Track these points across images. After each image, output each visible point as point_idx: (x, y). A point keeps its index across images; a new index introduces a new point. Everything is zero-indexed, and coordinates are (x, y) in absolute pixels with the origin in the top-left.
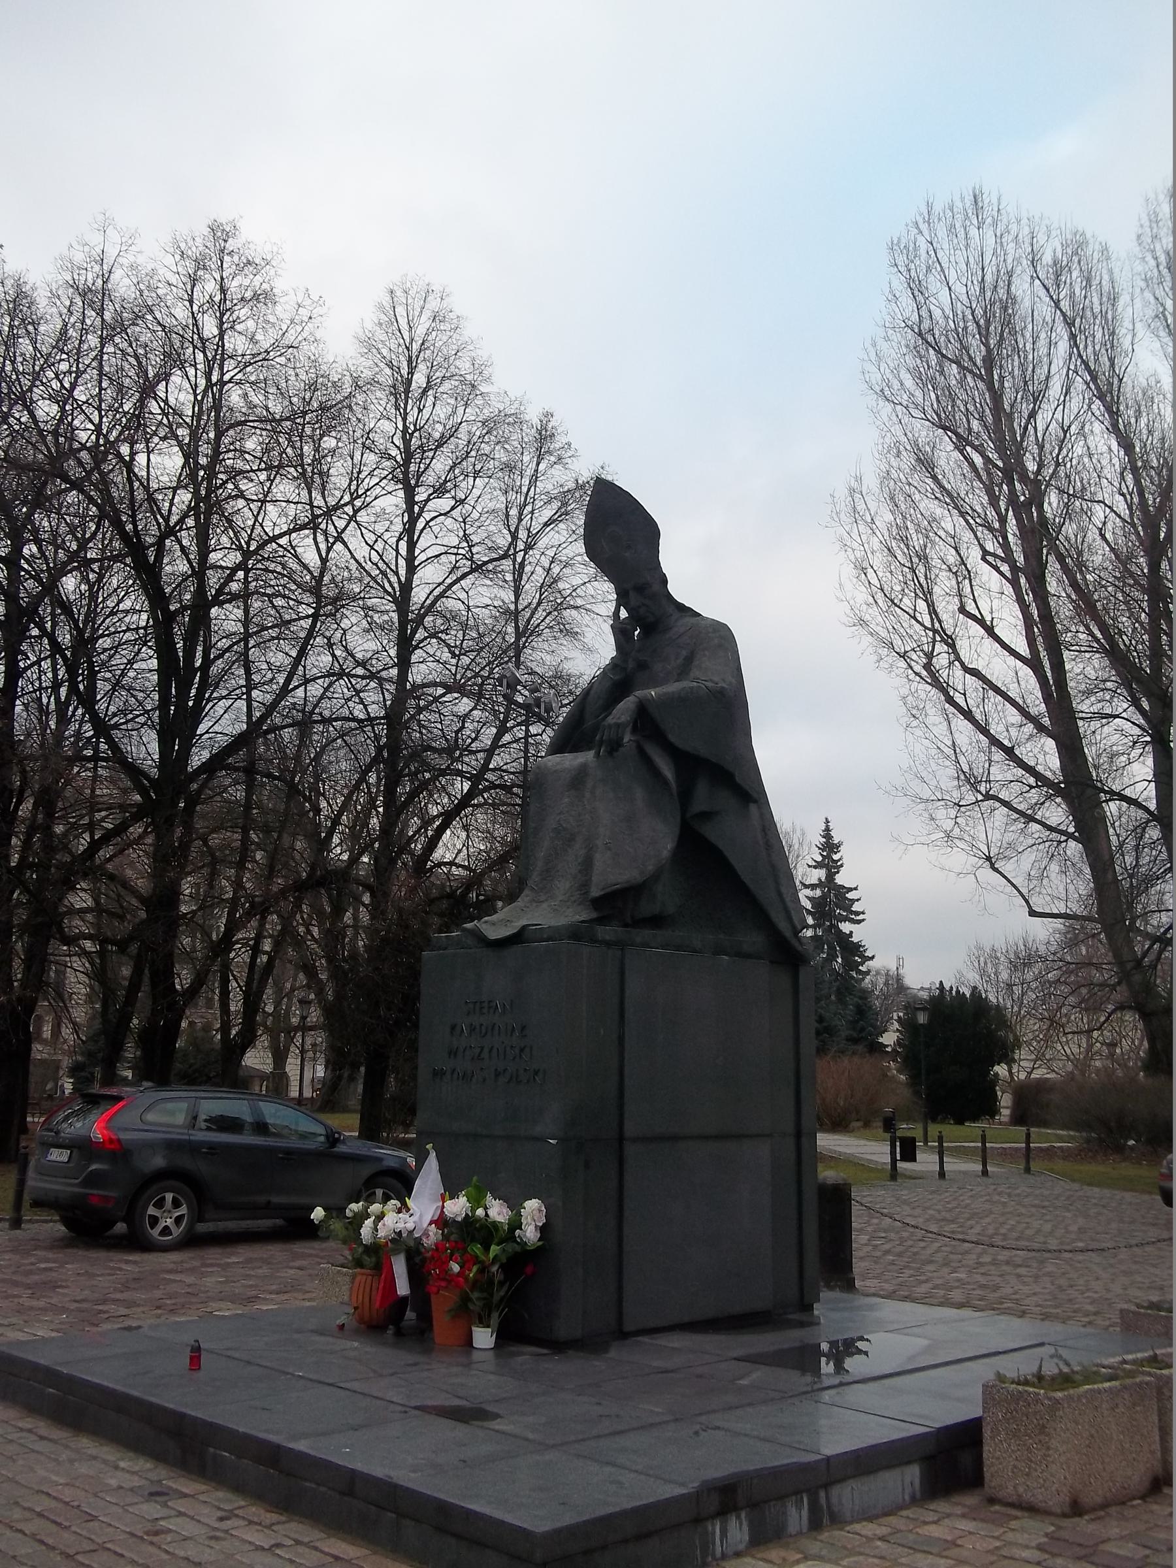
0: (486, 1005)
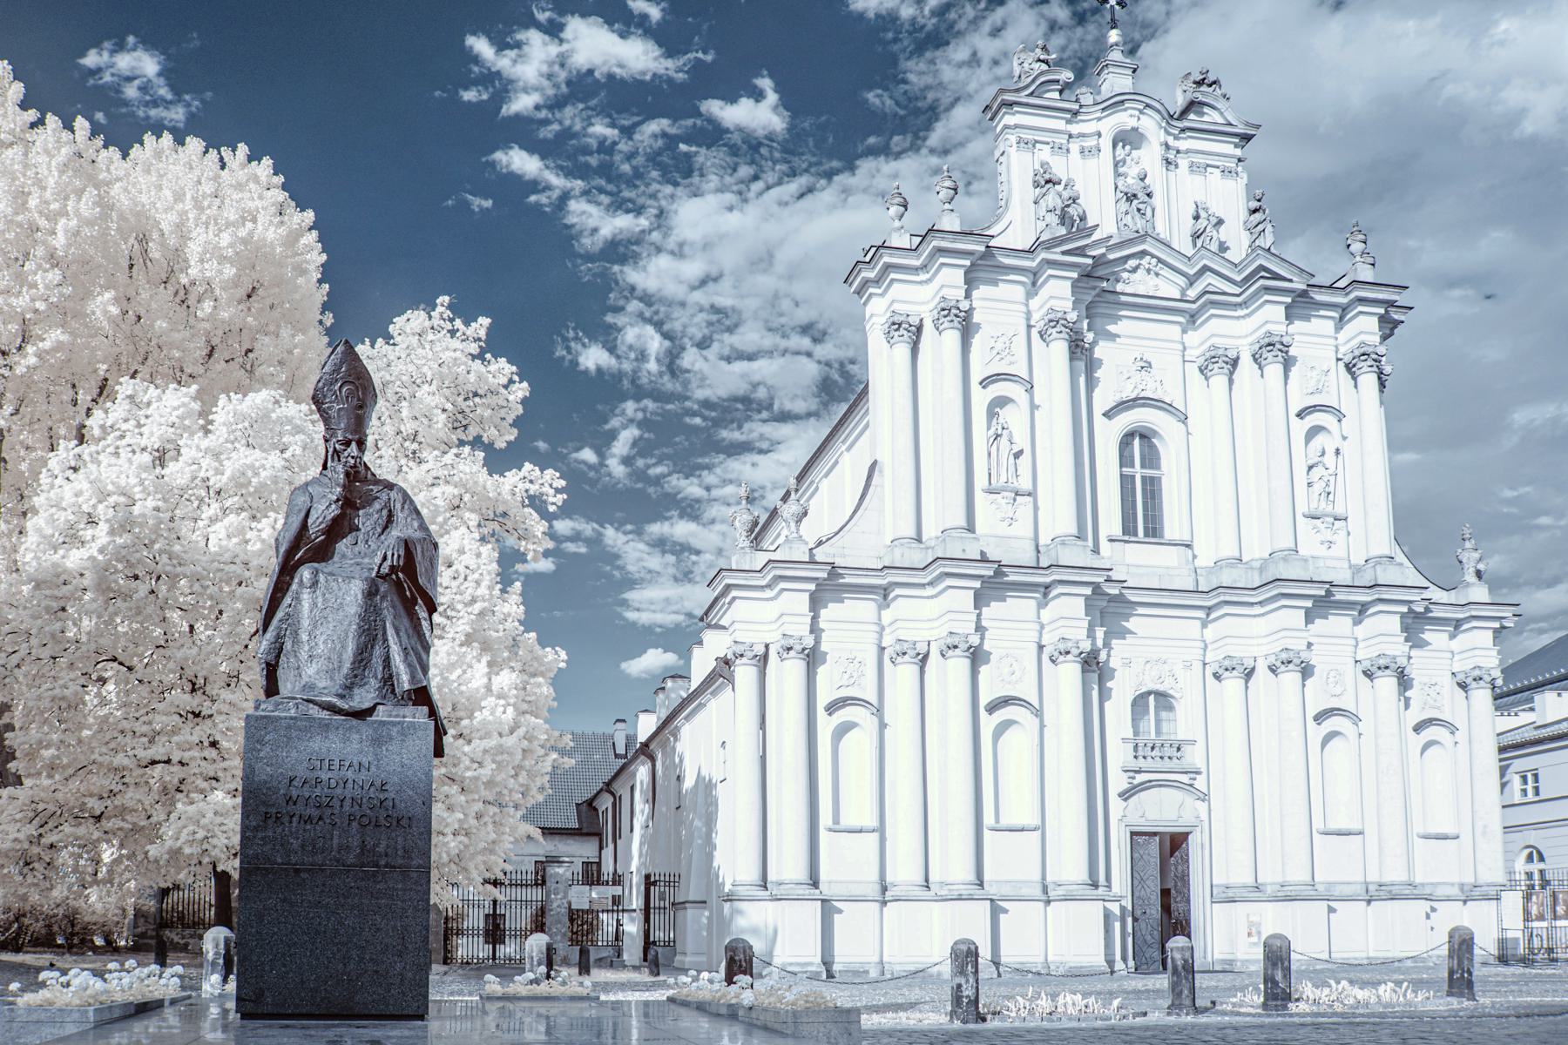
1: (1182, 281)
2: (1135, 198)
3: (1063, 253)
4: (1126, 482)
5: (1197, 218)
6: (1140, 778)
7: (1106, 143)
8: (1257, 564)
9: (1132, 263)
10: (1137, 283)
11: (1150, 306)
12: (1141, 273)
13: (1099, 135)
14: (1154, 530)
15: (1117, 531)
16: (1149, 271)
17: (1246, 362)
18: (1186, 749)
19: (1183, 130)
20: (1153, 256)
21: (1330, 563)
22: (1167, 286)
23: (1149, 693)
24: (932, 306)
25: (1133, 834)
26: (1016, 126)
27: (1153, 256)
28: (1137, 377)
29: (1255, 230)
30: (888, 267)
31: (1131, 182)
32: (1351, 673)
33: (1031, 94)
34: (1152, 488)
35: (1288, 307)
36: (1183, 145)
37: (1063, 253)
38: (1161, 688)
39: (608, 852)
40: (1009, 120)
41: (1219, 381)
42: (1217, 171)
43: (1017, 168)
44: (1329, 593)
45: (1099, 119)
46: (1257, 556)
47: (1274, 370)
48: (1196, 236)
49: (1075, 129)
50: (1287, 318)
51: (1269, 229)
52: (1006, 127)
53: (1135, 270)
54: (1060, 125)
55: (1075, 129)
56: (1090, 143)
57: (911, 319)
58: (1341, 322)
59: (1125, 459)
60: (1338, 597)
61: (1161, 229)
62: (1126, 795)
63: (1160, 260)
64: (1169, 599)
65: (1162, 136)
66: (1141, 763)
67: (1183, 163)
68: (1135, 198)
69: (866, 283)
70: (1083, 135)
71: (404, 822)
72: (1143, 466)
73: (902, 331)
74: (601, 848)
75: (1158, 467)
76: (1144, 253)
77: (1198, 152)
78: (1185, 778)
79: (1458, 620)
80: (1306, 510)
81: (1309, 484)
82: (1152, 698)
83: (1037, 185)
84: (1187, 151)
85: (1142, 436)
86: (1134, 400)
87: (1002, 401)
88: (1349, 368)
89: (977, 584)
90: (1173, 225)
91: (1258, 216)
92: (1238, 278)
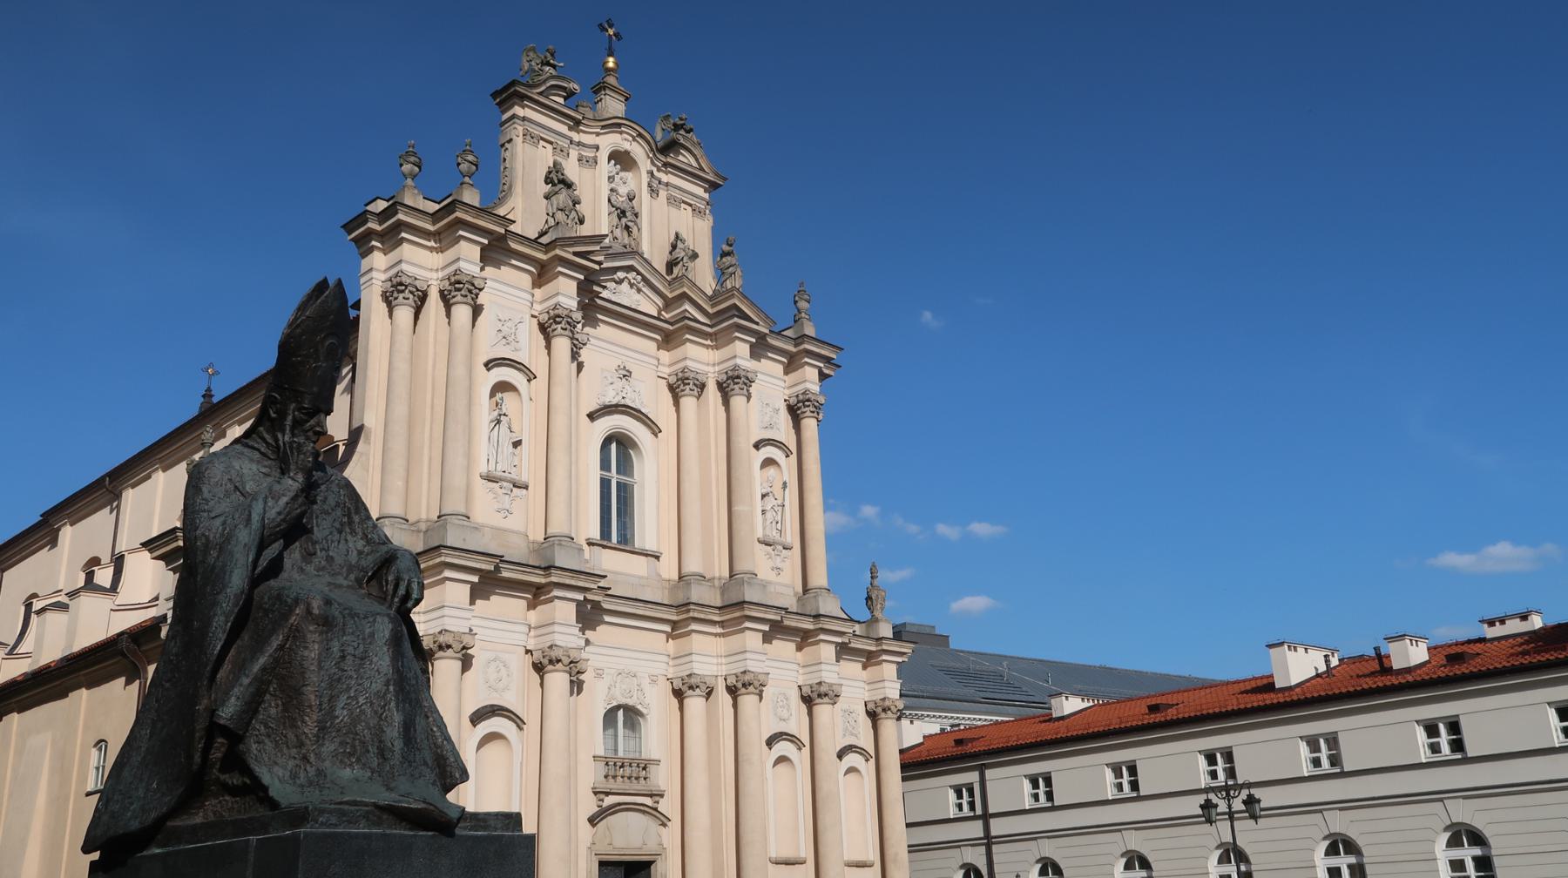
1: (660, 302)
2: (625, 214)
3: (575, 254)
4: (605, 484)
5: (674, 247)
6: (610, 800)
7: (603, 156)
8: (423, 527)
9: (621, 275)
10: (622, 293)
11: (629, 318)
12: (625, 285)
13: (597, 148)
14: (626, 543)
15: (595, 532)
16: (631, 285)
17: (434, 303)
18: (652, 768)
19: (666, 165)
20: (639, 273)
21: (780, 589)
22: (647, 304)
23: (618, 707)
24: (441, 275)
25: (602, 864)
26: (524, 119)
27: (639, 273)
28: (620, 384)
29: (721, 273)
30: (400, 226)
31: (621, 201)
32: (520, 666)
33: (540, 94)
34: (625, 492)
35: (484, 249)
36: (665, 178)
37: (575, 254)
38: (630, 702)
40: (518, 110)
41: (404, 314)
42: (549, 147)
43: (528, 161)
44: (497, 568)
45: (598, 134)
46: (424, 516)
47: (462, 312)
48: (670, 266)
49: (576, 137)
50: (482, 259)
51: (739, 273)
52: (514, 116)
53: (620, 282)
54: (563, 129)
55: (576, 137)
56: (589, 153)
57: (417, 283)
58: (788, 369)
59: (605, 465)
60: (505, 574)
61: (645, 248)
62: (593, 821)
63: (644, 279)
64: (638, 611)
65: (649, 166)
66: (611, 785)
67: (663, 193)
68: (625, 214)
69: (370, 234)
70: (584, 145)
72: (618, 472)
73: (407, 294)
75: (632, 476)
76: (630, 269)
77: (680, 189)
78: (648, 801)
79: (870, 652)
80: (483, 469)
81: (764, 512)
82: (621, 713)
83: (548, 180)
84: (667, 184)
85: (619, 443)
86: (617, 406)
87: (502, 387)
88: (543, 328)
89: (475, 579)
90: (653, 246)
91: (727, 260)
92: (432, 207)
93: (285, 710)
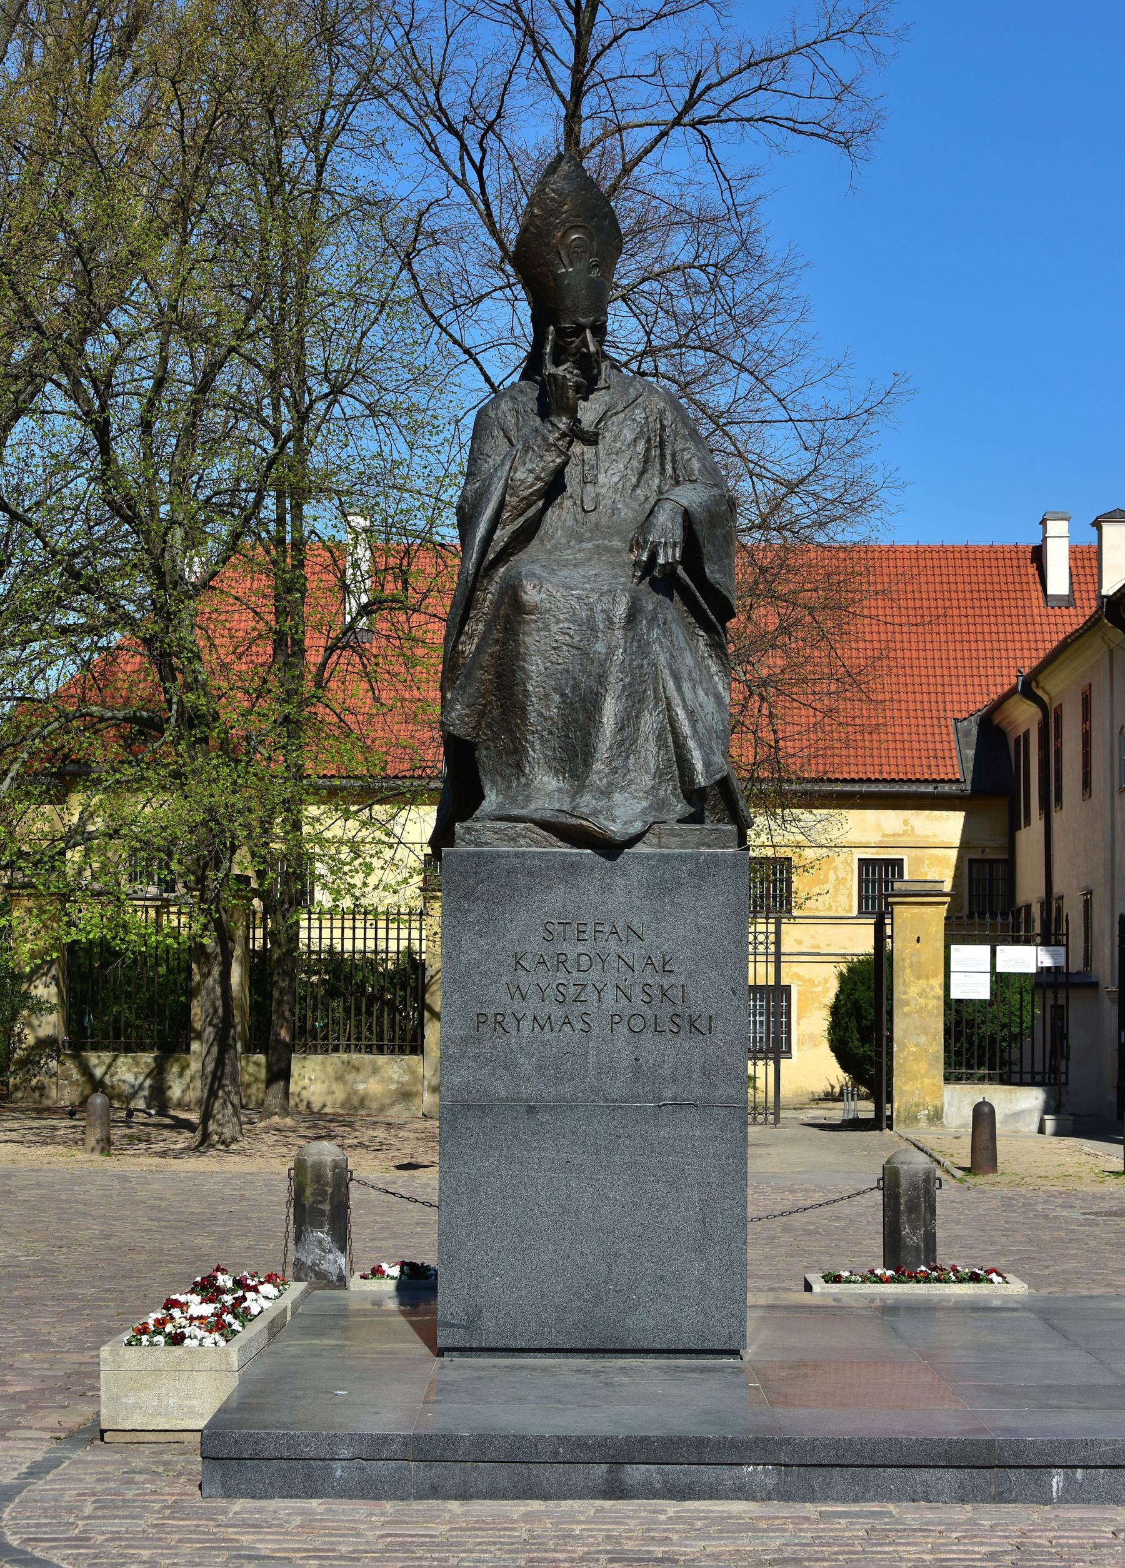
0: (589, 928)
39: (1030, 839)
71: (702, 1024)
74: (1014, 826)
93: (503, 713)
